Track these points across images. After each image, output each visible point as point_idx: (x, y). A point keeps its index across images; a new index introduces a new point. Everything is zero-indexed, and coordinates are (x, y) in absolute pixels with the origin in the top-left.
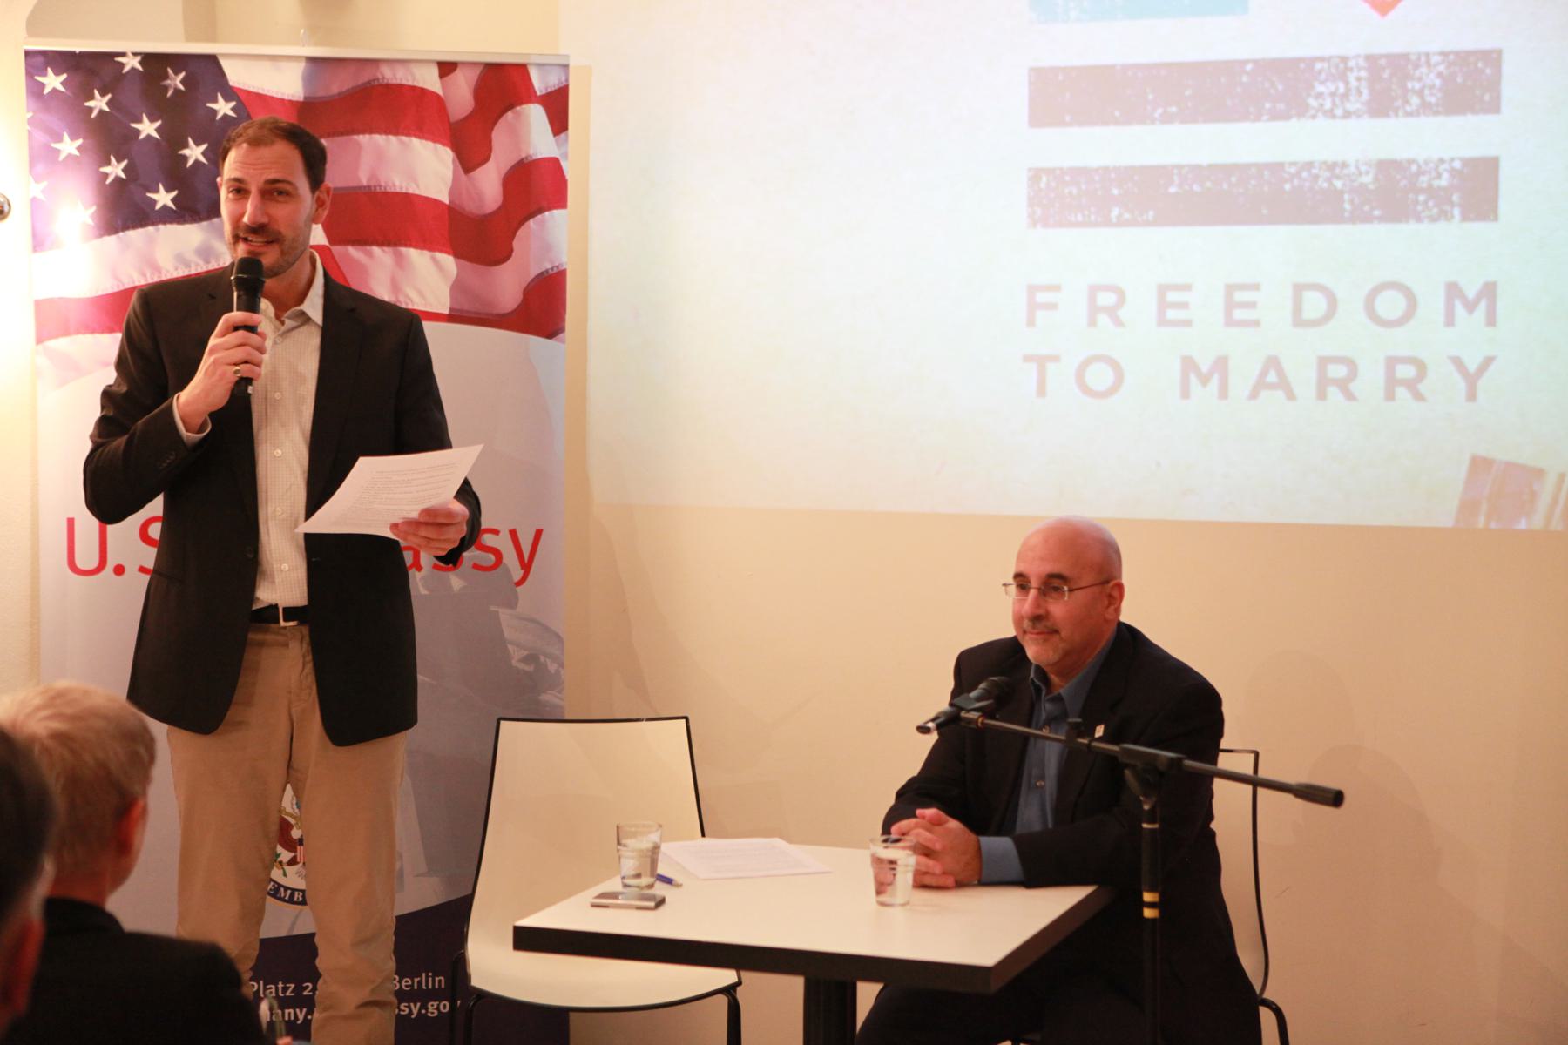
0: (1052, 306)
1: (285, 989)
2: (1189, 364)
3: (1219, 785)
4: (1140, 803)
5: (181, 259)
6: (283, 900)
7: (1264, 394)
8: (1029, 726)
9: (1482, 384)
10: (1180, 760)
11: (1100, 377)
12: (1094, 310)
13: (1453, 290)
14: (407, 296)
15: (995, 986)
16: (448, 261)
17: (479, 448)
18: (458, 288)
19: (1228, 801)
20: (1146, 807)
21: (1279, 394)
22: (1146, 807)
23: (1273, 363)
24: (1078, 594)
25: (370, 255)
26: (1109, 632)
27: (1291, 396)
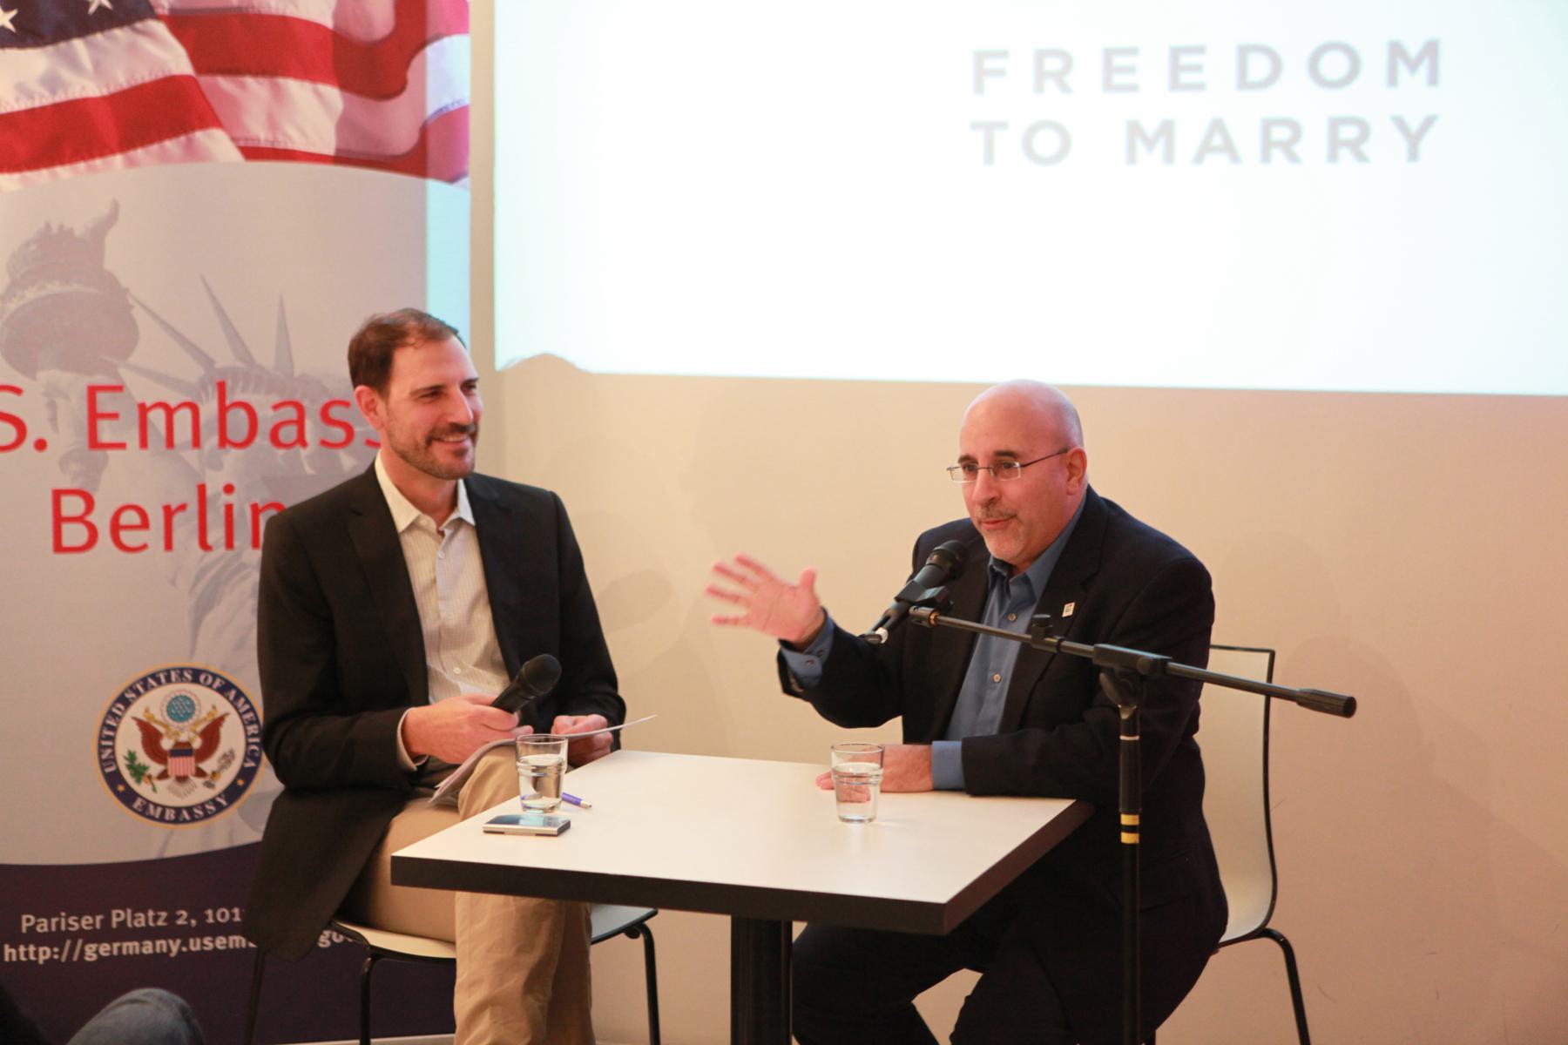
0: (1000, 73)
1: (156, 918)
2: (1134, 130)
3: (1210, 695)
4: (1117, 711)
5: (22, 89)
6: (152, 818)
7: (1210, 158)
8: (979, 620)
9: (1425, 145)
10: (1164, 662)
11: (1047, 143)
12: (1041, 75)
13: (1396, 51)
14: (286, 135)
15: (946, 928)
16: (333, 94)
18: (345, 124)
19: (1224, 725)
20: (1124, 716)
21: (1223, 158)
22: (1124, 716)
23: (1218, 126)
25: (243, 86)
26: (1075, 503)
27: (1235, 158)
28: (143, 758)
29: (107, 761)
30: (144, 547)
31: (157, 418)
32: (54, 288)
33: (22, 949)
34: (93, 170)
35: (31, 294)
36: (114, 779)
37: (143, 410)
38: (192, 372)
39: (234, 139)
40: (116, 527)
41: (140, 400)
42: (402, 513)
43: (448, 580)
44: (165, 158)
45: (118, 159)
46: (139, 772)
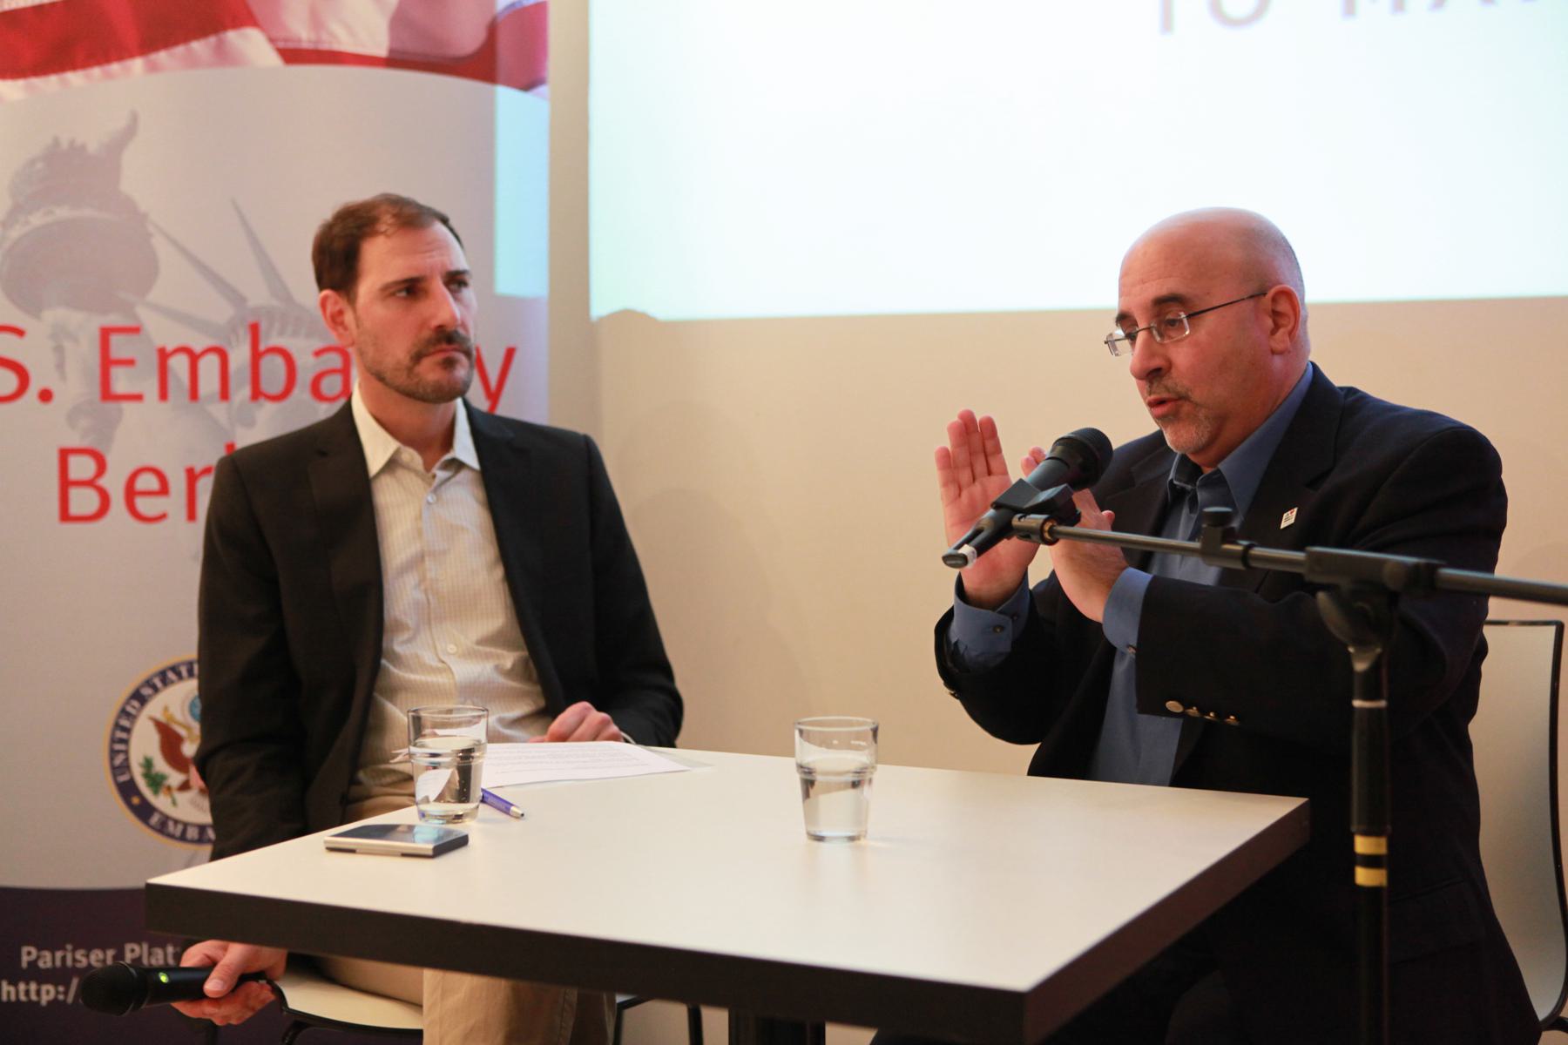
4: (1348, 661)
6: (171, 836)
17: (1214, 828)
20: (1360, 666)
22: (1360, 666)
24: (1210, 320)
28: (161, 766)
29: (120, 770)
30: (162, 517)
31: (179, 364)
32: (63, 213)
33: (22, 987)
34: (109, 76)
35: (37, 220)
36: (127, 790)
37: (164, 355)
38: (220, 312)
39: (272, 40)
40: (131, 493)
41: (159, 343)
42: (377, 446)
43: (436, 543)
44: (192, 62)
45: (137, 64)
46: (156, 782)
